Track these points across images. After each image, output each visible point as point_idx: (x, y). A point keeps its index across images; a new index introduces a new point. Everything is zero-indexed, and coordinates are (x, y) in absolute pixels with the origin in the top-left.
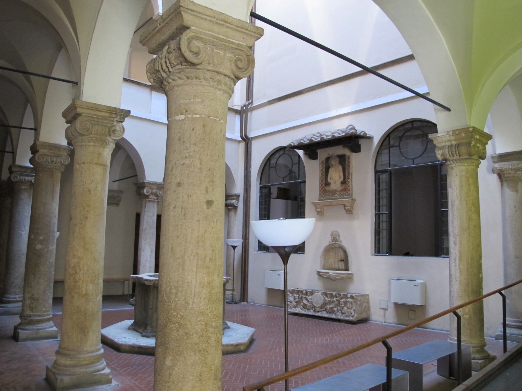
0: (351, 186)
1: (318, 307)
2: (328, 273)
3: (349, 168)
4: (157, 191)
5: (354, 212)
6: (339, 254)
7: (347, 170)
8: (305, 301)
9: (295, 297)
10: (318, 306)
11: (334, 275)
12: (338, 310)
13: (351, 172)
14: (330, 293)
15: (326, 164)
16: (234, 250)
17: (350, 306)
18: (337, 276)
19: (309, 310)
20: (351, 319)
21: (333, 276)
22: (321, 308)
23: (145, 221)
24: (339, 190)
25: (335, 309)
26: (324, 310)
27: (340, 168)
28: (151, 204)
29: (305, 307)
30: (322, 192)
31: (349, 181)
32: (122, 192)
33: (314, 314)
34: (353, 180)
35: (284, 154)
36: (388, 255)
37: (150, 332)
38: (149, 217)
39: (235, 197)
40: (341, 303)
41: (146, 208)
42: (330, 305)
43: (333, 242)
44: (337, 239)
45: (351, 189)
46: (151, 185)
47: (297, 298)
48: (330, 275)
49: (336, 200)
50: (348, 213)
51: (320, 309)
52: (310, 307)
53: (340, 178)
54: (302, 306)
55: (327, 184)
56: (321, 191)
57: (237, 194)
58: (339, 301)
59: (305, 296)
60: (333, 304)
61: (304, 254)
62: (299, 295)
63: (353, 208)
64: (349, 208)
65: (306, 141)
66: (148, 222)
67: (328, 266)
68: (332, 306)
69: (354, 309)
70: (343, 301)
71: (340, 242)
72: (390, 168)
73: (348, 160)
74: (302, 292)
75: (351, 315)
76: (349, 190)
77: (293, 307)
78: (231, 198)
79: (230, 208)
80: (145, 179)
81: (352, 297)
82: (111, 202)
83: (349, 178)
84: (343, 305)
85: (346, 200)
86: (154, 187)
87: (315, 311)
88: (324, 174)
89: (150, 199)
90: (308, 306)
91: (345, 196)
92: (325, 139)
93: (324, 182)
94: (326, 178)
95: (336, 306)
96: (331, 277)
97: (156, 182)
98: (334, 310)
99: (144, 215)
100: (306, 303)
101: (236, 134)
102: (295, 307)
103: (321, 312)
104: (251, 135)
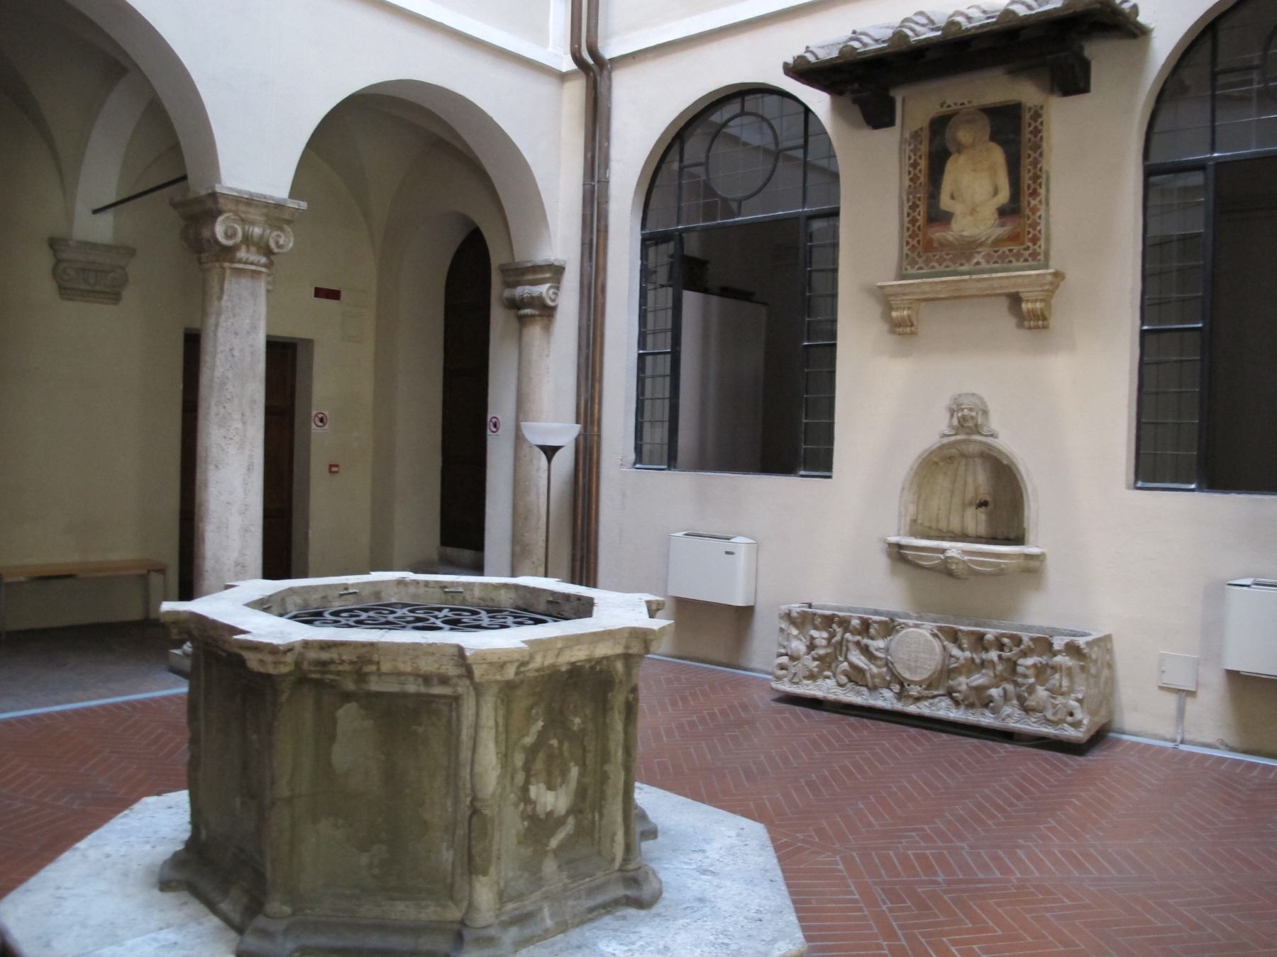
0: (1043, 222)
1: (915, 683)
2: (943, 551)
3: (1037, 155)
4: (269, 231)
5: (1053, 322)
6: (970, 480)
7: (1026, 163)
8: (857, 658)
9: (812, 638)
10: (917, 678)
11: (966, 558)
12: (1006, 697)
13: (1044, 169)
14: (972, 633)
15: (931, 141)
16: (549, 460)
17: (1065, 683)
18: (982, 564)
19: (873, 689)
20: (1070, 733)
21: (964, 562)
22: (929, 687)
23: (219, 350)
24: (990, 241)
25: (995, 692)
26: (941, 692)
27: (997, 155)
28: (245, 282)
29: (856, 677)
30: (913, 249)
31: (1035, 205)
32: (131, 252)
33: (898, 706)
34: (1053, 202)
35: (743, 113)
36: (1193, 486)
37: (287, 931)
38: (236, 334)
39: (548, 275)
40: (1020, 669)
41: (225, 297)
42: (969, 673)
43: (956, 434)
44: (976, 425)
45: (1043, 236)
46: (242, 208)
47: (824, 642)
48: (951, 558)
49: (986, 276)
50: (1030, 328)
51: (925, 689)
52: (877, 681)
53: (996, 192)
54: (845, 673)
55: (939, 217)
56: (908, 243)
57: (556, 264)
58: (1012, 665)
59: (858, 638)
60: (984, 671)
61: (830, 477)
62: (832, 635)
63: (1050, 305)
64: (1038, 305)
65: (872, 45)
66: (233, 356)
67: (927, 524)
68: (978, 679)
69: (1080, 696)
70: (1035, 665)
71: (992, 435)
72: (1216, 155)
73: (1033, 125)
74: (844, 623)
75: (1069, 719)
76: (1035, 240)
77: (804, 678)
78: (530, 277)
79: (527, 311)
80: (218, 180)
81: (1072, 650)
82: (87, 287)
83: (1034, 194)
84: (1032, 680)
85: (1030, 276)
86: (254, 214)
87: (900, 696)
88: (923, 179)
89: (240, 261)
90: (873, 676)
91: (1018, 260)
92: (968, 30)
93: (922, 209)
94: (934, 194)
95: (999, 680)
96: (954, 567)
97: (265, 197)
98: (991, 696)
99: (217, 325)
100: (861, 665)
101: (550, 49)
102: (812, 677)
103: (931, 701)
104: (610, 50)
